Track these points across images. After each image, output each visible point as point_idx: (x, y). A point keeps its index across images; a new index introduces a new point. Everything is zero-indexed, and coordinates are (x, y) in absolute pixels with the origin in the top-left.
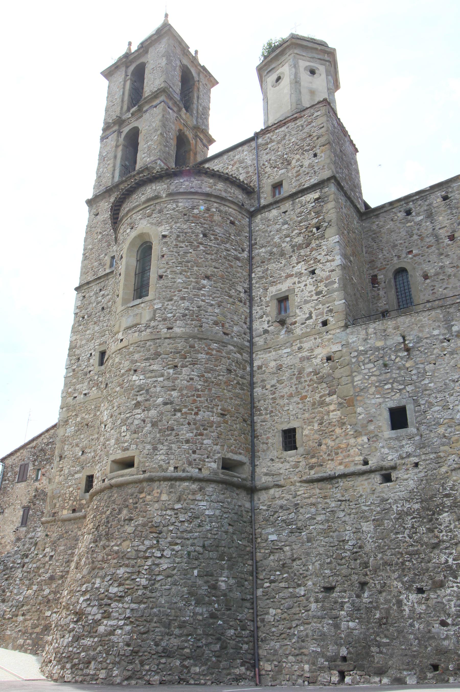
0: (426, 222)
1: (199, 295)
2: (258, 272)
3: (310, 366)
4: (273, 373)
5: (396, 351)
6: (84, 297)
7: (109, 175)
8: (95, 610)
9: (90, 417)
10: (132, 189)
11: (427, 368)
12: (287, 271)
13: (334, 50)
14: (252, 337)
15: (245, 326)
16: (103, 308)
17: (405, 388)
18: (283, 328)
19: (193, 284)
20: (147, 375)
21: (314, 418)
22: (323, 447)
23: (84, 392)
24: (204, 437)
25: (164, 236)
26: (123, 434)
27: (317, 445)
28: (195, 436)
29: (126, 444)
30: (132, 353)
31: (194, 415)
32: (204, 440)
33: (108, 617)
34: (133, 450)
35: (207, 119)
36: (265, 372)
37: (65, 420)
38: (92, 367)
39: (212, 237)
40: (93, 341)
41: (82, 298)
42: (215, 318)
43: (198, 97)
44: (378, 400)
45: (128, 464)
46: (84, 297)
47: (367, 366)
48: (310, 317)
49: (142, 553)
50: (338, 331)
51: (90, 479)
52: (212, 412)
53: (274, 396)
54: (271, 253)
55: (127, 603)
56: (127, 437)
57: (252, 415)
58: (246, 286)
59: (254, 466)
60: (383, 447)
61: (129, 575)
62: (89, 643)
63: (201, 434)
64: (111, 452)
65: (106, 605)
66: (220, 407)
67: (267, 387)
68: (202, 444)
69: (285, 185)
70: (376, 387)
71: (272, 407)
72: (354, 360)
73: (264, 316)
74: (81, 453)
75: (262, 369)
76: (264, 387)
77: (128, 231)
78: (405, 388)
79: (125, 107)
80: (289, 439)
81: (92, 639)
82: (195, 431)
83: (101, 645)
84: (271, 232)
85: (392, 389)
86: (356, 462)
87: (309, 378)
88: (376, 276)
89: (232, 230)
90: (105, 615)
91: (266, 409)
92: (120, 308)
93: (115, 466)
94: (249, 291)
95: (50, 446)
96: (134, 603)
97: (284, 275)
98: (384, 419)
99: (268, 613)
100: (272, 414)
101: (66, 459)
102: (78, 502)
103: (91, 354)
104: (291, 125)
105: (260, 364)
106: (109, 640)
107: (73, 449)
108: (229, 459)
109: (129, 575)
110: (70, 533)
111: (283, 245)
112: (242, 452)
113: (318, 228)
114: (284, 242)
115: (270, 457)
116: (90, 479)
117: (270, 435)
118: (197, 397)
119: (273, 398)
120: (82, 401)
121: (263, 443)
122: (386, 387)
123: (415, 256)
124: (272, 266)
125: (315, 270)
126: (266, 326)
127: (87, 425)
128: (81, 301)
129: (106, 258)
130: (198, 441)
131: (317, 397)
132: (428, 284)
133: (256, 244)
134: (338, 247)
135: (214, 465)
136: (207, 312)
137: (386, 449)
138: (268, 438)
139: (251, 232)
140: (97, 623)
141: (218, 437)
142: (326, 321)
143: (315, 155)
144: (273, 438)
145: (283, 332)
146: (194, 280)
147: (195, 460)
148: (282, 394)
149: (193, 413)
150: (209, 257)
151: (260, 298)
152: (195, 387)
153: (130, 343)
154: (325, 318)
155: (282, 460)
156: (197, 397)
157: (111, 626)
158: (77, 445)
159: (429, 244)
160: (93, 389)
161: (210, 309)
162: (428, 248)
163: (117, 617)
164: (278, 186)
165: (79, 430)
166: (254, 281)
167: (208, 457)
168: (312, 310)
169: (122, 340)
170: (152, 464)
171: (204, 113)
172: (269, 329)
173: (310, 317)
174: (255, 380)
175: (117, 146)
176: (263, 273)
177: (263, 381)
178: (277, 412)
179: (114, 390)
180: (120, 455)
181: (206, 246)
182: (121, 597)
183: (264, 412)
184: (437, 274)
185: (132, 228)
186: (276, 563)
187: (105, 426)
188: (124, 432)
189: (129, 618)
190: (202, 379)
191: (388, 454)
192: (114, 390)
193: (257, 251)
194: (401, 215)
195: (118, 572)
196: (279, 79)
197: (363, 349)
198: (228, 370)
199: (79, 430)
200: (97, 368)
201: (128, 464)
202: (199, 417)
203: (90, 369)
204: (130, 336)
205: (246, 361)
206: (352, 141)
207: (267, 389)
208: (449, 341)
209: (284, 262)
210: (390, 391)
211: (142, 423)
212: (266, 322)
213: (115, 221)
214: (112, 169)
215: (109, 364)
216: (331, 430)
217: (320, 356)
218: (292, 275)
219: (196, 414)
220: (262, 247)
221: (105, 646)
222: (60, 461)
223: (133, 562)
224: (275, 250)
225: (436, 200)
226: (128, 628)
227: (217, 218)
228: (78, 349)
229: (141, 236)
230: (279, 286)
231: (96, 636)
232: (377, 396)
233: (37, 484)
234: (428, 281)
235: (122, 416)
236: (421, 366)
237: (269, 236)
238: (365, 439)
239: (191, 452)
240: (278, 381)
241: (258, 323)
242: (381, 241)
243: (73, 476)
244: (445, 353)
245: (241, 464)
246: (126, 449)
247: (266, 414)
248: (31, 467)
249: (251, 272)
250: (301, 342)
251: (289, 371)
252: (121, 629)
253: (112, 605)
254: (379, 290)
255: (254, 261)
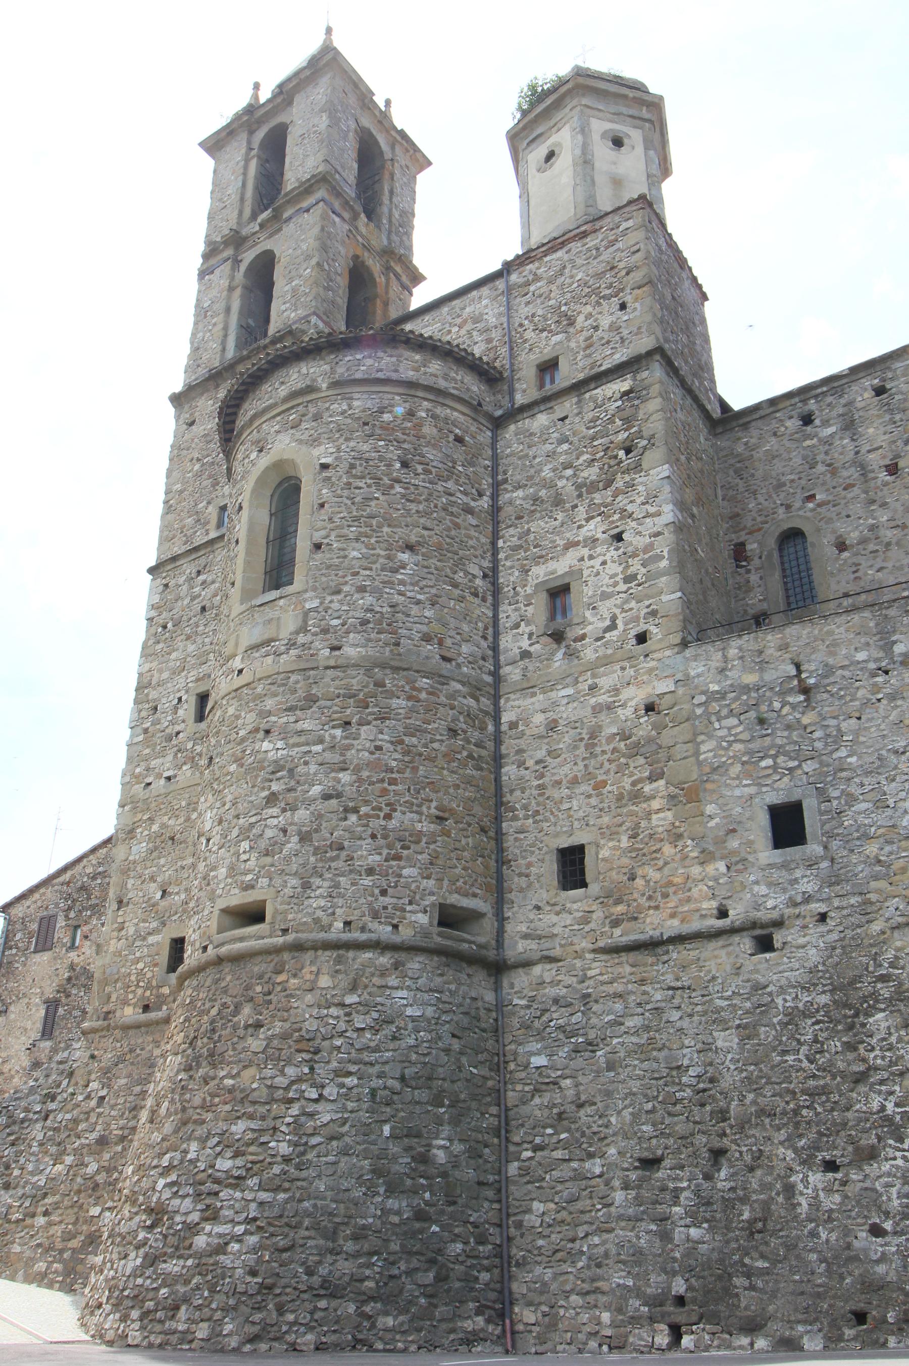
0: (841, 438)
1: (392, 583)
2: (510, 537)
3: (612, 722)
4: (539, 737)
5: (783, 694)
6: (166, 586)
7: (215, 345)
8: (187, 1203)
9: (178, 822)
10: (260, 373)
11: (844, 726)
12: (568, 535)
13: (661, 98)
14: (497, 666)
15: (484, 644)
16: (203, 609)
17: (799, 766)
18: (559, 648)
19: (381, 560)
20: (291, 741)
21: (620, 825)
22: (639, 882)
23: (166, 774)
24: (402, 863)
25: (325, 467)
26: (244, 857)
27: (626, 878)
28: (386, 860)
29: (249, 877)
30: (261, 697)
31: (384, 818)
32: (404, 868)
33: (214, 1219)
34: (262, 888)
35: (409, 235)
36: (523, 734)
37: (128, 828)
38: (183, 725)
39: (420, 468)
40: (183, 674)
41: (161, 588)
42: (424, 628)
43: (391, 192)
44: (746, 789)
45: (254, 915)
46: (166, 586)
47: (725, 723)
48: (613, 626)
49: (281, 1092)
50: (668, 653)
51: (178, 945)
52: (420, 813)
53: (541, 782)
54: (536, 500)
55: (252, 1190)
56: (252, 864)
57: (498, 820)
58: (486, 564)
59: (501, 919)
60: (757, 883)
61: (256, 1135)
62: (176, 1269)
63: (398, 857)
64: (219, 892)
65: (209, 1194)
66: (434, 804)
67: (527, 765)
68: (400, 876)
69: (564, 365)
70: (743, 763)
71: (538, 804)
72: (699, 711)
73: (523, 623)
74: (159, 894)
75: (517, 728)
76: (521, 764)
77: (253, 455)
78: (799, 766)
79: (247, 212)
80: (572, 866)
81: (181, 1262)
82: (385, 852)
83: (200, 1274)
84: (535, 457)
85: (775, 767)
86: (704, 912)
87: (611, 747)
88: (743, 544)
89: (459, 454)
90: (207, 1214)
91: (525, 807)
92: (237, 608)
93: (227, 920)
94: (492, 575)
95: (99, 881)
96: (265, 1190)
97: (562, 543)
98: (759, 827)
99: (529, 1211)
100: (537, 818)
101: (131, 906)
102: (154, 992)
103: (180, 699)
104: (575, 246)
105: (514, 719)
106: (216, 1263)
107: (144, 886)
108: (453, 906)
109: (256, 1135)
110: (138, 1051)
111: (560, 484)
112: (479, 891)
113: (628, 451)
114: (561, 478)
115: (534, 902)
116: (178, 945)
117: (533, 859)
118: (389, 784)
119: (539, 786)
120: (163, 791)
121: (520, 875)
122: (763, 764)
123: (819, 505)
124: (538, 526)
125: (622, 533)
126: (525, 644)
127: (172, 839)
128: (161, 593)
129: (210, 508)
130: (390, 871)
131: (627, 783)
132: (845, 560)
133: (505, 481)
134: (667, 489)
135: (423, 919)
136: (408, 616)
137: (763, 887)
138: (529, 865)
139: (495, 458)
140: (192, 1229)
141: (431, 864)
142: (645, 633)
143: (623, 307)
144: (540, 864)
145: (560, 655)
146: (383, 553)
147: (385, 908)
148: (557, 778)
149: (382, 815)
150: (413, 507)
151: (514, 589)
152: (386, 765)
153: (257, 676)
154: (642, 627)
155: (557, 908)
156: (389, 784)
157: (220, 1236)
158: (152, 879)
159: (848, 481)
160: (185, 768)
161: (415, 610)
162: (845, 489)
163: (230, 1218)
164: (549, 367)
165: (156, 848)
166: (501, 556)
167: (410, 903)
168: (617, 611)
169: (240, 671)
170: (300, 916)
171: (404, 224)
172: (532, 649)
173: (613, 626)
174: (504, 750)
175: (231, 289)
176: (519, 539)
177: (520, 751)
178: (548, 814)
179: (225, 771)
180: (237, 898)
181: (407, 486)
182: (238, 1178)
183: (521, 814)
184: (863, 541)
185: (261, 451)
186: (546, 1112)
187: (208, 840)
188: (244, 852)
189: (255, 1219)
190: (399, 748)
191: (766, 895)
192: (225, 771)
193: (507, 496)
194: (793, 424)
195: (234, 1128)
196: (550, 156)
197: (716, 688)
198: (450, 729)
199: (156, 848)
200: (191, 726)
201: (254, 915)
202: (393, 823)
203: (178, 728)
204: (257, 664)
205: (487, 713)
206: (695, 279)
207: (527, 769)
208: (886, 672)
209: (560, 516)
210: (770, 771)
211: (282, 834)
212: (526, 636)
213: (227, 436)
214: (221, 333)
215: (216, 718)
216: (654, 848)
217: (633, 703)
218: (577, 544)
219: (388, 817)
220: (518, 487)
221: (207, 1275)
222: (118, 909)
223: (262, 1109)
224: (543, 493)
225: (862, 394)
226: (253, 1240)
227: (428, 430)
228: (154, 688)
229: (278, 465)
230: (552, 565)
231: (190, 1256)
232: (745, 782)
233: (73, 955)
234: (846, 554)
235: (241, 821)
236: (833, 722)
237: (532, 466)
238: (721, 866)
239: (377, 891)
240: (549, 753)
241: (509, 638)
242: (753, 475)
243: (144, 939)
244: (880, 696)
245: (477, 916)
246: (249, 887)
247: (526, 817)
248: (61, 922)
249: (495, 536)
250: (594, 676)
251: (572, 732)
252: (240, 1241)
253: (221, 1194)
254: (748, 572)
255: (502, 515)
